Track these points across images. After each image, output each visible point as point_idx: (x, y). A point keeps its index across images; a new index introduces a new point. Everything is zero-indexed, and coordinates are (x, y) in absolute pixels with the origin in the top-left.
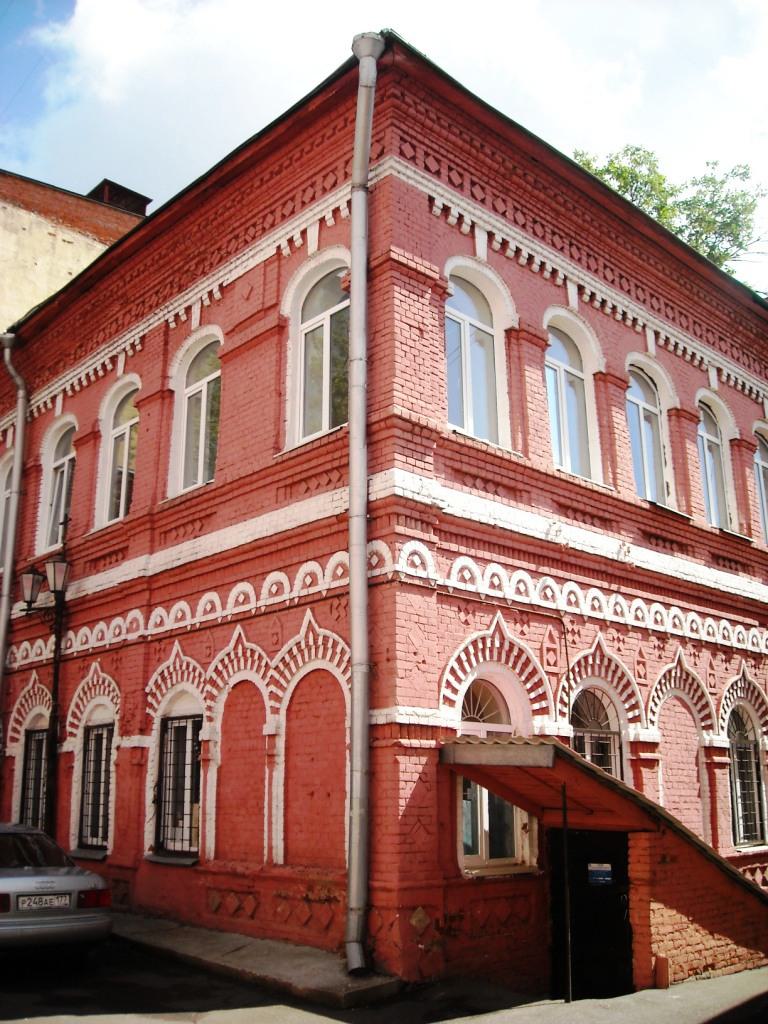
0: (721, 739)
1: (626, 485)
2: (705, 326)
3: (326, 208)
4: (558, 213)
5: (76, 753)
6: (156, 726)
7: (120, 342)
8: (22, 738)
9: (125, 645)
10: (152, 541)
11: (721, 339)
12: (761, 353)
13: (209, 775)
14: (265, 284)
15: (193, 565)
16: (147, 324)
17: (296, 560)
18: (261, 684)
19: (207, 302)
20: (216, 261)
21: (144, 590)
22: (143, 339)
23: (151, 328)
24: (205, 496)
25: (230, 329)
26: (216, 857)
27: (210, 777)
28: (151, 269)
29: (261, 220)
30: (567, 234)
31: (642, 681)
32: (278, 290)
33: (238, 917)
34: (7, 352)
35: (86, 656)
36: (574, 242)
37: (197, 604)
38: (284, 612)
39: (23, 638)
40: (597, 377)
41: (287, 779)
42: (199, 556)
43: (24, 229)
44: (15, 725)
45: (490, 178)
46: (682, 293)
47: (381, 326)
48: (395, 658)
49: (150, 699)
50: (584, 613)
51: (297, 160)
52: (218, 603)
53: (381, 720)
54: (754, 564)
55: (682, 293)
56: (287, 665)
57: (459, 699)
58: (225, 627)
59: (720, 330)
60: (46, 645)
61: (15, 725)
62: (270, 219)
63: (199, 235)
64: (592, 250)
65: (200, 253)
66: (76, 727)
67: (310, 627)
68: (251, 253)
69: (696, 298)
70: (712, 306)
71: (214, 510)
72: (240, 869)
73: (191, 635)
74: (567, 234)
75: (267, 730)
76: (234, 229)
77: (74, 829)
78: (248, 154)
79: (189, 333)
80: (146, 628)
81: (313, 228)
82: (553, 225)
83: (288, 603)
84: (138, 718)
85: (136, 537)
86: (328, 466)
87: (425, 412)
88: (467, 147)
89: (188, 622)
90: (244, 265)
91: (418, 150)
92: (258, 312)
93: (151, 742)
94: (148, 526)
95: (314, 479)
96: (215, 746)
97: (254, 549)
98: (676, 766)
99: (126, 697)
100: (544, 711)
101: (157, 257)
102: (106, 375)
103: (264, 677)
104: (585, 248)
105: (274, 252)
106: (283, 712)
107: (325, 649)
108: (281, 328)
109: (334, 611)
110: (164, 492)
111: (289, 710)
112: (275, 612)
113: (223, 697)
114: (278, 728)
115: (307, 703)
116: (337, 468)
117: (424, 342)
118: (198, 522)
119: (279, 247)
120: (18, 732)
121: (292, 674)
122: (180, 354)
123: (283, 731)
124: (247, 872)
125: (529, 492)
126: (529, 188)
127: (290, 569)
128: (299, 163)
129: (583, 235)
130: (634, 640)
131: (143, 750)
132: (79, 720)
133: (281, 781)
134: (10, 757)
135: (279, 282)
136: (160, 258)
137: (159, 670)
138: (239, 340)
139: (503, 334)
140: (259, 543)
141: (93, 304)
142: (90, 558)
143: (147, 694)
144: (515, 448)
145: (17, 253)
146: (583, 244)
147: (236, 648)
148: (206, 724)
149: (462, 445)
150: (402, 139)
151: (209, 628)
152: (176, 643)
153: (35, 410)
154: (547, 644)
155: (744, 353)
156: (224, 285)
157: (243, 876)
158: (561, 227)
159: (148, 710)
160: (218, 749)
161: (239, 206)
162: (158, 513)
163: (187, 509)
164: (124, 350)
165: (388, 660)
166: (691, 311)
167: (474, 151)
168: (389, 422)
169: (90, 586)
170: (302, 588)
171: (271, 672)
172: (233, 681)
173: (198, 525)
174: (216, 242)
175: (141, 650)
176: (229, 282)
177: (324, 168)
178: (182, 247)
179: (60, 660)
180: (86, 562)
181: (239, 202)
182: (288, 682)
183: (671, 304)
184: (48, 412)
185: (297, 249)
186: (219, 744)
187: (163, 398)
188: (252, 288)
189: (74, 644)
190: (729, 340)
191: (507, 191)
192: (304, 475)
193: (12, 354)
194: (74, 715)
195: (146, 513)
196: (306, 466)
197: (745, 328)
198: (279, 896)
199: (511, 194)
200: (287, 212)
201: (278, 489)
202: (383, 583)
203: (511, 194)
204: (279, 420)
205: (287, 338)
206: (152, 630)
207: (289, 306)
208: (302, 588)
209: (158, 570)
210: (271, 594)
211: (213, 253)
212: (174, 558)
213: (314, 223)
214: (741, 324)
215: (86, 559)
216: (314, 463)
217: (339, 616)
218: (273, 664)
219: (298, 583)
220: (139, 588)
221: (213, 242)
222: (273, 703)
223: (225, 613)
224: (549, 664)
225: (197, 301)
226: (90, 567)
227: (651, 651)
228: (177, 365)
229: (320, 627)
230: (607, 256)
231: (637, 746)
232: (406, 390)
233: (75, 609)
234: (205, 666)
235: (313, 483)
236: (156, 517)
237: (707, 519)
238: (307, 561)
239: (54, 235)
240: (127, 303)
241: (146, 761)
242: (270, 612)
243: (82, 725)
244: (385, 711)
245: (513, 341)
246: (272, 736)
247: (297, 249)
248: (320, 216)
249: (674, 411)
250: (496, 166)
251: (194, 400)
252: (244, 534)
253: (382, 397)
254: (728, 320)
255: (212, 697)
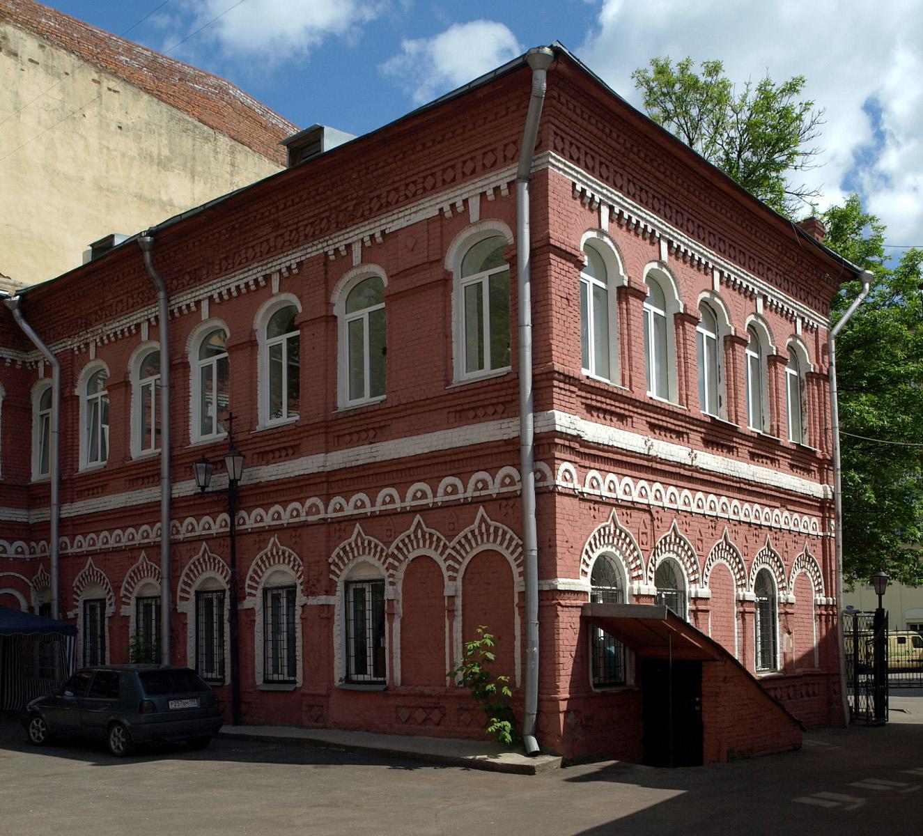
0: (751, 595)
1: (694, 404)
2: (757, 260)
3: (489, 184)
4: (658, 179)
5: (257, 609)
6: (340, 587)
7: (275, 263)
8: (192, 597)
9: (305, 525)
10: (327, 442)
11: (769, 269)
12: (799, 277)
13: (455, 624)
14: (428, 240)
15: (372, 466)
16: (304, 252)
17: (469, 469)
18: (440, 560)
19: (368, 244)
20: (376, 209)
21: (323, 482)
22: (300, 265)
23: (308, 256)
24: (380, 412)
25: (394, 272)
26: (402, 685)
27: (394, 629)
28: (307, 202)
29: (422, 180)
30: (663, 196)
31: (700, 553)
32: (442, 248)
33: (426, 725)
34: (147, 256)
35: (262, 533)
36: (668, 202)
37: (377, 496)
38: (458, 507)
39: (188, 514)
40: (677, 317)
41: (464, 627)
42: (378, 459)
43: (67, 74)
44: (183, 587)
45: (612, 157)
46: (743, 235)
47: (541, 298)
48: (556, 546)
49: (332, 567)
50: (665, 505)
51: (459, 135)
52: (396, 496)
53: (546, 588)
54: (779, 458)
55: (743, 235)
56: (462, 546)
57: (589, 570)
58: (404, 515)
59: (769, 261)
60: (215, 522)
61: (183, 587)
62: (430, 181)
63: (358, 181)
64: (680, 206)
65: (357, 197)
66: (256, 589)
67: (483, 519)
68: (414, 210)
69: (753, 237)
70: (765, 242)
71: (388, 423)
72: (427, 691)
73: (371, 520)
74: (663, 196)
75: (448, 592)
76: (394, 182)
77: (259, 668)
78: (416, 122)
79: (350, 267)
80: (326, 513)
81: (474, 198)
82: (654, 190)
83: (462, 501)
84: (324, 582)
85: (310, 438)
86: (495, 401)
87: (571, 364)
88: (600, 134)
89: (368, 509)
90: (407, 218)
91: (565, 141)
92: (424, 263)
93: (337, 600)
94: (323, 430)
95: (481, 409)
96: (398, 604)
97: (429, 458)
98: (719, 614)
99: (309, 566)
100: (639, 577)
101: (313, 193)
102: (260, 290)
103: (442, 554)
104: (675, 206)
105: (437, 213)
106: (459, 580)
107: (488, 535)
108: (446, 281)
109: (503, 509)
110: (335, 403)
111: (464, 578)
112: (451, 506)
113: (404, 567)
114: (456, 591)
115: (479, 573)
116: (502, 403)
117: (570, 309)
118: (372, 431)
119: (441, 210)
120: (188, 593)
121: (467, 553)
122: (341, 284)
123: (460, 594)
124: (433, 694)
125: (631, 417)
126: (640, 162)
127: (464, 477)
128: (460, 137)
129: (675, 195)
130: (696, 524)
131: (330, 608)
132: (257, 583)
133: (460, 629)
134: (182, 613)
135: (442, 241)
136: (317, 194)
137: (342, 545)
138: (404, 284)
139: (615, 290)
140: (435, 454)
141: (241, 223)
142: (258, 450)
143: (330, 564)
144: (623, 385)
145: (63, 101)
146: (674, 203)
147: (415, 532)
148: (388, 588)
149: (593, 387)
150: (555, 133)
151: (389, 515)
152: (358, 525)
153: (176, 310)
154: (643, 530)
155: (785, 279)
156: (387, 232)
157: (430, 696)
158: (659, 190)
159: (331, 576)
160: (400, 606)
161: (399, 164)
162: (332, 420)
163: (360, 420)
164: (280, 271)
165: (550, 547)
166: (748, 248)
167: (604, 137)
168: (549, 376)
169: (264, 475)
170: (475, 491)
171: (449, 551)
172: (411, 557)
173: (372, 433)
174: (375, 190)
175: (323, 529)
176: (392, 230)
177: (485, 146)
178: (340, 188)
179: (234, 536)
180: (253, 454)
181: (400, 160)
182: (463, 558)
183: (733, 244)
184: (192, 315)
185: (459, 218)
186: (401, 602)
187: (327, 322)
188: (416, 242)
189: (248, 521)
190: (775, 270)
191: (623, 166)
192: (472, 405)
193: (152, 256)
194: (252, 579)
195: (321, 419)
196: (474, 398)
197: (788, 257)
198: (462, 709)
199: (627, 168)
200: (448, 177)
201: (449, 412)
202: (545, 493)
203: (627, 168)
204: (447, 357)
205: (452, 290)
206: (331, 514)
207: (452, 261)
208: (475, 491)
209: (336, 467)
210: (446, 493)
211: (372, 199)
212: (352, 458)
213: (476, 195)
214: (785, 255)
215: (254, 451)
216: (481, 397)
217: (507, 513)
218: (451, 545)
219: (471, 486)
220: (318, 480)
221: (372, 189)
222: (450, 573)
223: (403, 505)
224: (643, 544)
225: (358, 241)
226: (258, 458)
227: (707, 530)
228: (338, 294)
229: (491, 520)
230: (690, 211)
231: (696, 599)
232: (560, 350)
233: (246, 493)
234: (388, 544)
235: (481, 412)
236: (330, 424)
237: (750, 427)
238: (478, 471)
239: (99, 83)
240: (278, 226)
241: (333, 615)
242: (446, 506)
243: (260, 587)
244: (549, 581)
245: (623, 295)
246: (452, 598)
247: (459, 218)
248: (481, 191)
249: (729, 338)
250: (618, 147)
251: (356, 325)
252: (422, 445)
253: (543, 355)
254: (776, 253)
255: (395, 568)
